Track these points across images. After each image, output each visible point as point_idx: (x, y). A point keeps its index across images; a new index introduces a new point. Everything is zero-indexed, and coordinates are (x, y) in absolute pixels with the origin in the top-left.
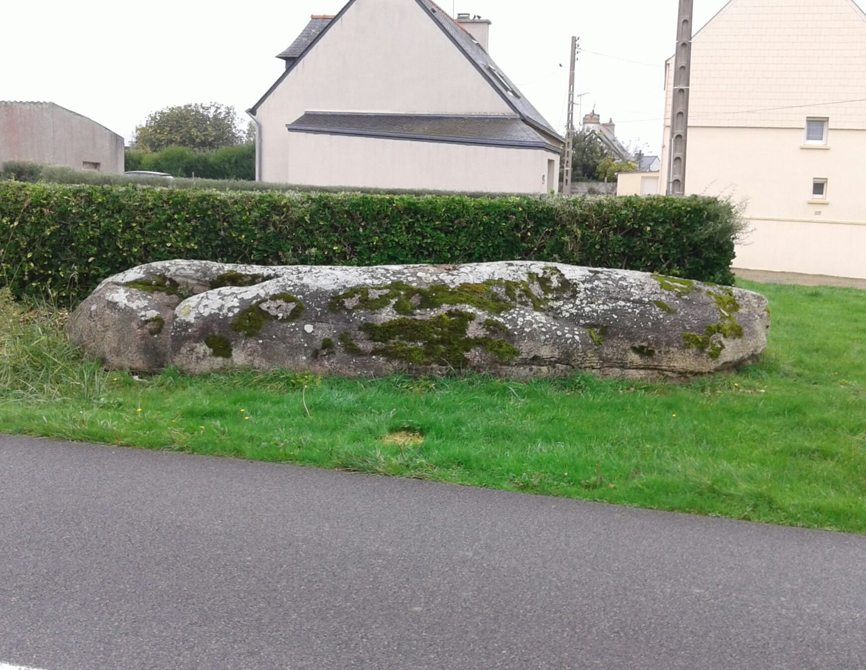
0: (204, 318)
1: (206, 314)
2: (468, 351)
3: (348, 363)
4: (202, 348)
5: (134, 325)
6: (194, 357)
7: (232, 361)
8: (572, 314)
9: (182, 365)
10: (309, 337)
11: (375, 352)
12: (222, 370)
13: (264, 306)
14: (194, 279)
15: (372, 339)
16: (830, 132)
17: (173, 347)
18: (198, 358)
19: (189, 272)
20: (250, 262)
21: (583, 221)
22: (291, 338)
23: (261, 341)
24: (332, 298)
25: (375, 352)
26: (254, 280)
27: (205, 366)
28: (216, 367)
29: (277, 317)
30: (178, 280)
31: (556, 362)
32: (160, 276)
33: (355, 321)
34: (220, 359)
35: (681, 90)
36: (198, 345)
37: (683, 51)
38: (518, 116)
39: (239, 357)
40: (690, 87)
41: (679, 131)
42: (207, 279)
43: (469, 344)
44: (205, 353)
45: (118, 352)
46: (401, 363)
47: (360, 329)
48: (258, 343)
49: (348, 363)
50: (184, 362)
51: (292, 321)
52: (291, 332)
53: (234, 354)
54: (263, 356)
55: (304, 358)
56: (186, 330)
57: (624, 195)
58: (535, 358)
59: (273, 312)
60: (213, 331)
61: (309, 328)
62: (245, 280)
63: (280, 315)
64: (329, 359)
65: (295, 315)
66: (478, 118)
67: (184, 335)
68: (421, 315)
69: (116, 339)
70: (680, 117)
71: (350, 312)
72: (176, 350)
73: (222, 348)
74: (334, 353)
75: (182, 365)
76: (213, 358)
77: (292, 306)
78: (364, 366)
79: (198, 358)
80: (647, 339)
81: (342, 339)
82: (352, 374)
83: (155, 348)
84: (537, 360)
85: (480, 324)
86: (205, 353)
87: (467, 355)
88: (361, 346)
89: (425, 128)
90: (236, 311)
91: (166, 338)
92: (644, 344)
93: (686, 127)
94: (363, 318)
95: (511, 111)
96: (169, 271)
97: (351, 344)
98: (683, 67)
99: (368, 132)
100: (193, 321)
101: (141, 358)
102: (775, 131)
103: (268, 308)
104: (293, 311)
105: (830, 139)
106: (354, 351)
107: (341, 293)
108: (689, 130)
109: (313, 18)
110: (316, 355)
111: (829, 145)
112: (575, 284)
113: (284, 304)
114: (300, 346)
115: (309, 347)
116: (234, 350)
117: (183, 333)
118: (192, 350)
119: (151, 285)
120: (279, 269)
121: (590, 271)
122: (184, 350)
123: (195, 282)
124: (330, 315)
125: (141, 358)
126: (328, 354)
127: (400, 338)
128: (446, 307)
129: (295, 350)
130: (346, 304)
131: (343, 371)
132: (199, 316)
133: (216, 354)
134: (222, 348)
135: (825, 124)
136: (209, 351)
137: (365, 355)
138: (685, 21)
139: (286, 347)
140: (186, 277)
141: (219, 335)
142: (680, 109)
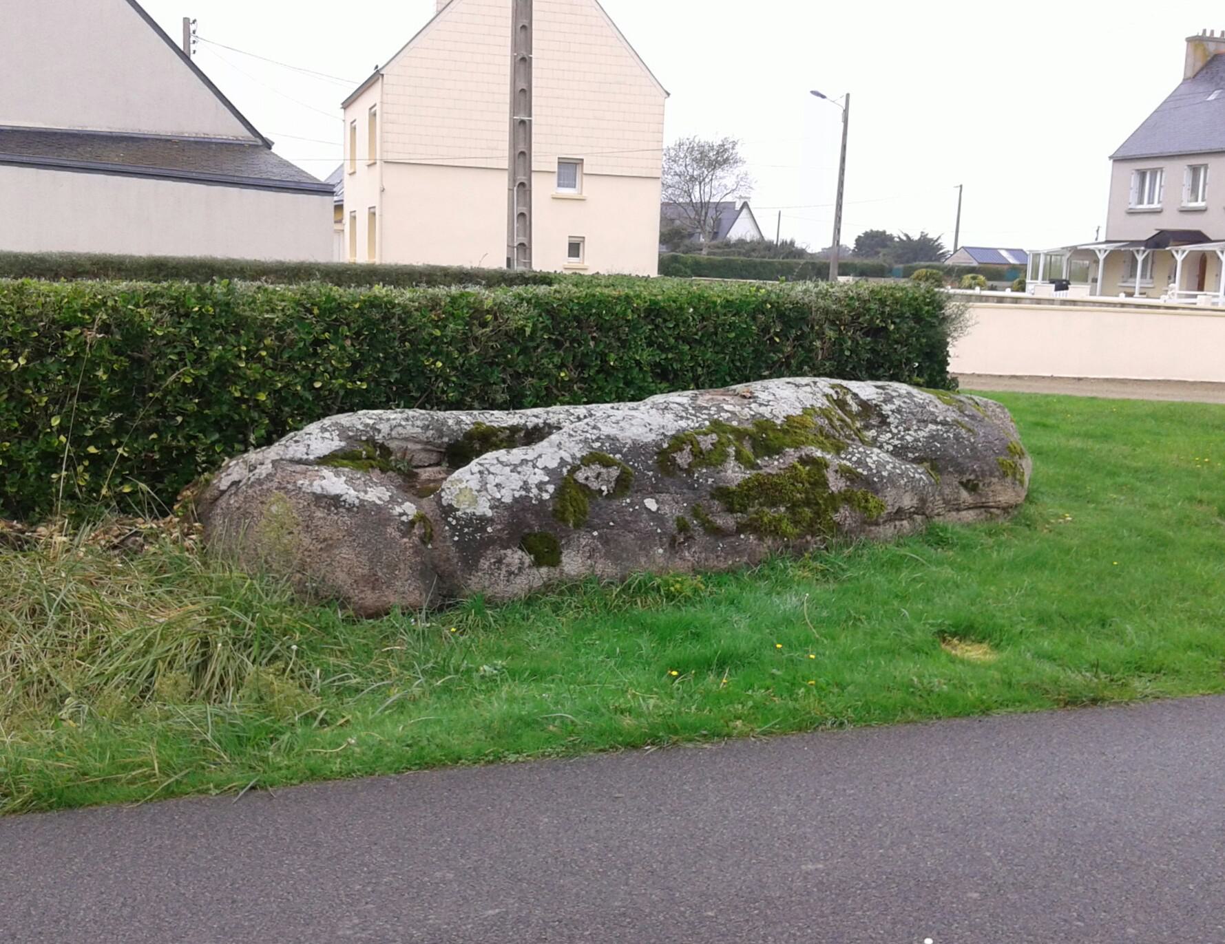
0: (508, 507)
1: (508, 500)
2: (837, 511)
3: (714, 550)
4: (515, 556)
5: (391, 531)
6: (503, 572)
7: (562, 572)
8: (895, 446)
9: (484, 588)
10: (656, 516)
11: (741, 529)
12: (548, 587)
13: (580, 476)
14: (419, 442)
15: (731, 510)
16: (585, 178)
17: (465, 560)
18: (510, 573)
19: (411, 430)
20: (494, 406)
21: (834, 319)
22: (636, 522)
23: (595, 533)
24: (657, 453)
25: (741, 529)
26: (534, 435)
27: (520, 585)
28: (537, 583)
29: (601, 491)
30: (393, 445)
31: (914, 513)
32: (367, 440)
33: (700, 485)
34: (544, 570)
35: (523, 122)
36: (509, 552)
37: (522, 67)
38: (260, 142)
39: (572, 563)
40: (533, 119)
41: (521, 178)
42: (446, 440)
43: (834, 501)
44: (522, 563)
45: (373, 582)
46: (775, 540)
47: (713, 497)
48: (594, 537)
49: (714, 550)
50: (487, 584)
51: (623, 496)
52: (631, 514)
53: (564, 559)
54: (607, 556)
55: (661, 551)
56: (483, 530)
57: (626, 273)
58: (900, 510)
59: (594, 485)
60: (531, 527)
61: (651, 504)
62: (502, 436)
63: (604, 488)
64: (689, 547)
65: (623, 484)
66: (196, 142)
67: (475, 539)
68: (773, 466)
69: (364, 559)
70: (522, 158)
71: (689, 472)
72: (470, 563)
73: (545, 552)
74: (692, 537)
75: (484, 588)
76: (534, 570)
77: (615, 472)
78: (736, 551)
79: (510, 573)
80: (974, 471)
81: (696, 515)
82: (722, 565)
83: (435, 567)
84: (899, 514)
85: (836, 471)
86: (522, 563)
87: (837, 517)
88: (720, 522)
89: (115, 157)
90: (551, 488)
91: (447, 547)
92: (972, 477)
93: (529, 172)
94: (710, 481)
95: (248, 134)
96: (379, 431)
97: (709, 522)
98: (523, 90)
99: (25, 159)
100: (489, 513)
101: (417, 588)
102: (546, 175)
103: (587, 479)
104: (619, 480)
105: (588, 187)
106: (717, 532)
107: (665, 446)
108: (533, 175)
109: (1189, 40)
110: (673, 546)
111: (585, 194)
112: (876, 405)
113: (603, 470)
114: (652, 534)
115: (664, 533)
116: (565, 552)
117: (478, 536)
118: (499, 561)
119: (360, 458)
120: (556, 413)
121: (833, 387)
122: (484, 564)
123: (419, 447)
124: (668, 481)
125: (417, 588)
126: (686, 539)
127: (761, 505)
128: (792, 456)
129: (646, 539)
130: (679, 461)
131: (711, 563)
132: (496, 504)
133: (538, 563)
134: (545, 552)
135: (579, 168)
136: (528, 559)
137: (731, 535)
138: (524, 27)
139: (637, 538)
140: (406, 439)
141: (537, 528)
142: (522, 148)
